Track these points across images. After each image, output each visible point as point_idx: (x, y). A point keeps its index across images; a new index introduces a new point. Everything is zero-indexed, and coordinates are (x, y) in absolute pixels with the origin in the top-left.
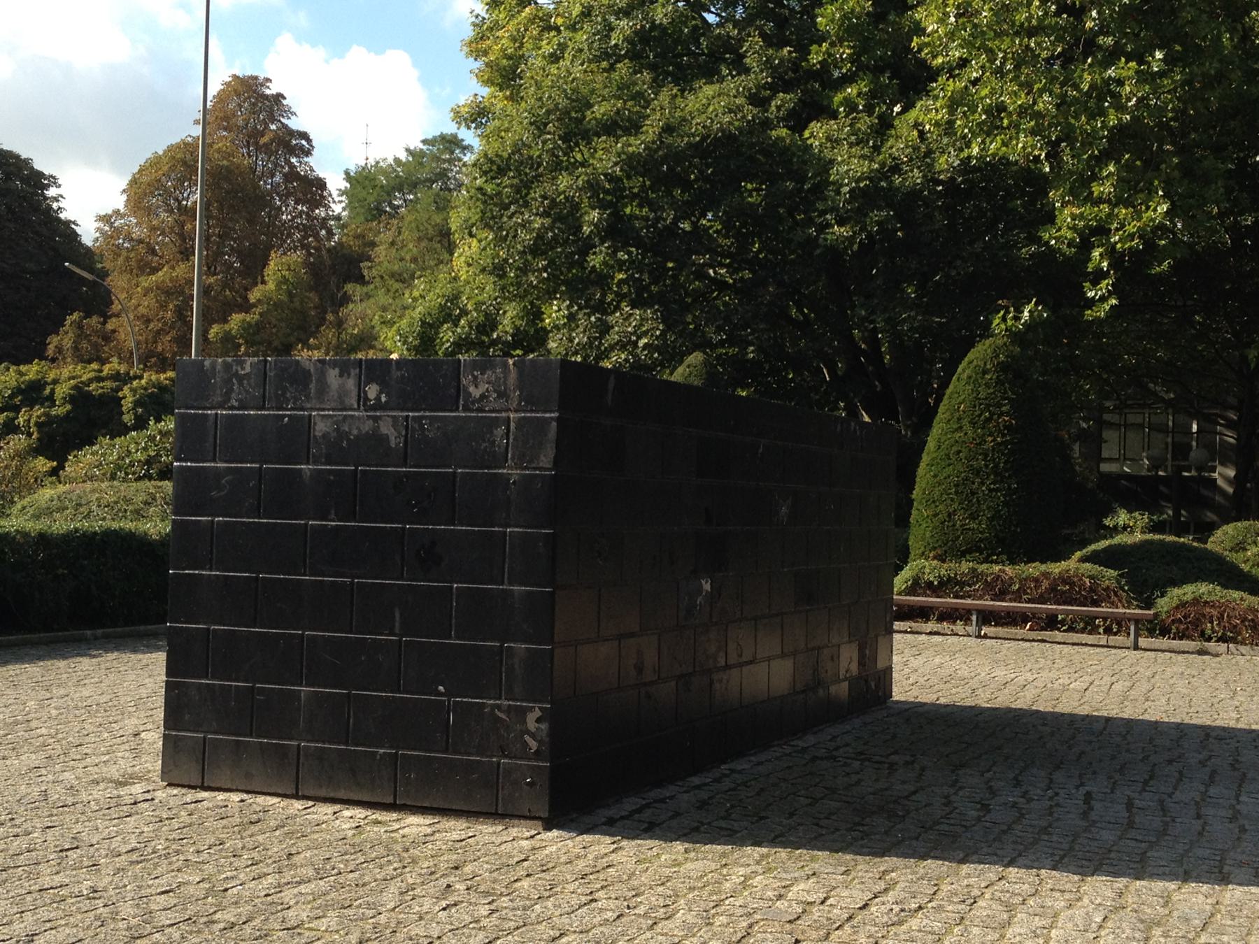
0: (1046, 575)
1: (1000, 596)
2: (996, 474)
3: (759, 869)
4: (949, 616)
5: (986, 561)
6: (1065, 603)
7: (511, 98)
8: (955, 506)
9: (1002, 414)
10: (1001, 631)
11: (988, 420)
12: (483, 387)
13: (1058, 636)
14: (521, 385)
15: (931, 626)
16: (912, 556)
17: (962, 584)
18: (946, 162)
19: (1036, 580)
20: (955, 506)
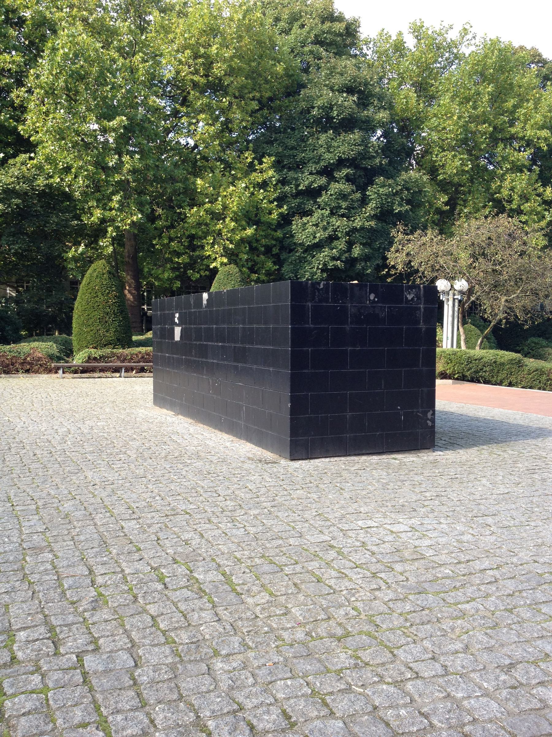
0: (140, 352)
1: (123, 361)
2: (115, 314)
3: (218, 503)
4: (102, 370)
5: (114, 348)
6: (147, 362)
7: (536, 123)
8: (100, 327)
9: (113, 291)
10: (101, 374)
11: (108, 293)
12: (412, 296)
13: (146, 375)
14: (425, 295)
15: (96, 375)
16: (75, 349)
17: (108, 357)
18: (41, 182)
19: (136, 355)
20: (100, 327)
